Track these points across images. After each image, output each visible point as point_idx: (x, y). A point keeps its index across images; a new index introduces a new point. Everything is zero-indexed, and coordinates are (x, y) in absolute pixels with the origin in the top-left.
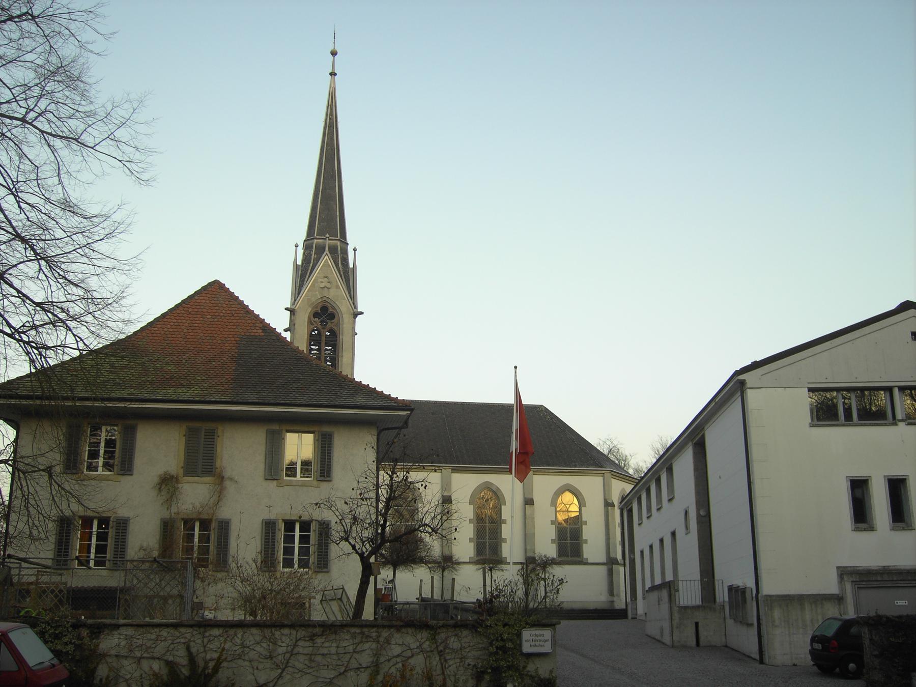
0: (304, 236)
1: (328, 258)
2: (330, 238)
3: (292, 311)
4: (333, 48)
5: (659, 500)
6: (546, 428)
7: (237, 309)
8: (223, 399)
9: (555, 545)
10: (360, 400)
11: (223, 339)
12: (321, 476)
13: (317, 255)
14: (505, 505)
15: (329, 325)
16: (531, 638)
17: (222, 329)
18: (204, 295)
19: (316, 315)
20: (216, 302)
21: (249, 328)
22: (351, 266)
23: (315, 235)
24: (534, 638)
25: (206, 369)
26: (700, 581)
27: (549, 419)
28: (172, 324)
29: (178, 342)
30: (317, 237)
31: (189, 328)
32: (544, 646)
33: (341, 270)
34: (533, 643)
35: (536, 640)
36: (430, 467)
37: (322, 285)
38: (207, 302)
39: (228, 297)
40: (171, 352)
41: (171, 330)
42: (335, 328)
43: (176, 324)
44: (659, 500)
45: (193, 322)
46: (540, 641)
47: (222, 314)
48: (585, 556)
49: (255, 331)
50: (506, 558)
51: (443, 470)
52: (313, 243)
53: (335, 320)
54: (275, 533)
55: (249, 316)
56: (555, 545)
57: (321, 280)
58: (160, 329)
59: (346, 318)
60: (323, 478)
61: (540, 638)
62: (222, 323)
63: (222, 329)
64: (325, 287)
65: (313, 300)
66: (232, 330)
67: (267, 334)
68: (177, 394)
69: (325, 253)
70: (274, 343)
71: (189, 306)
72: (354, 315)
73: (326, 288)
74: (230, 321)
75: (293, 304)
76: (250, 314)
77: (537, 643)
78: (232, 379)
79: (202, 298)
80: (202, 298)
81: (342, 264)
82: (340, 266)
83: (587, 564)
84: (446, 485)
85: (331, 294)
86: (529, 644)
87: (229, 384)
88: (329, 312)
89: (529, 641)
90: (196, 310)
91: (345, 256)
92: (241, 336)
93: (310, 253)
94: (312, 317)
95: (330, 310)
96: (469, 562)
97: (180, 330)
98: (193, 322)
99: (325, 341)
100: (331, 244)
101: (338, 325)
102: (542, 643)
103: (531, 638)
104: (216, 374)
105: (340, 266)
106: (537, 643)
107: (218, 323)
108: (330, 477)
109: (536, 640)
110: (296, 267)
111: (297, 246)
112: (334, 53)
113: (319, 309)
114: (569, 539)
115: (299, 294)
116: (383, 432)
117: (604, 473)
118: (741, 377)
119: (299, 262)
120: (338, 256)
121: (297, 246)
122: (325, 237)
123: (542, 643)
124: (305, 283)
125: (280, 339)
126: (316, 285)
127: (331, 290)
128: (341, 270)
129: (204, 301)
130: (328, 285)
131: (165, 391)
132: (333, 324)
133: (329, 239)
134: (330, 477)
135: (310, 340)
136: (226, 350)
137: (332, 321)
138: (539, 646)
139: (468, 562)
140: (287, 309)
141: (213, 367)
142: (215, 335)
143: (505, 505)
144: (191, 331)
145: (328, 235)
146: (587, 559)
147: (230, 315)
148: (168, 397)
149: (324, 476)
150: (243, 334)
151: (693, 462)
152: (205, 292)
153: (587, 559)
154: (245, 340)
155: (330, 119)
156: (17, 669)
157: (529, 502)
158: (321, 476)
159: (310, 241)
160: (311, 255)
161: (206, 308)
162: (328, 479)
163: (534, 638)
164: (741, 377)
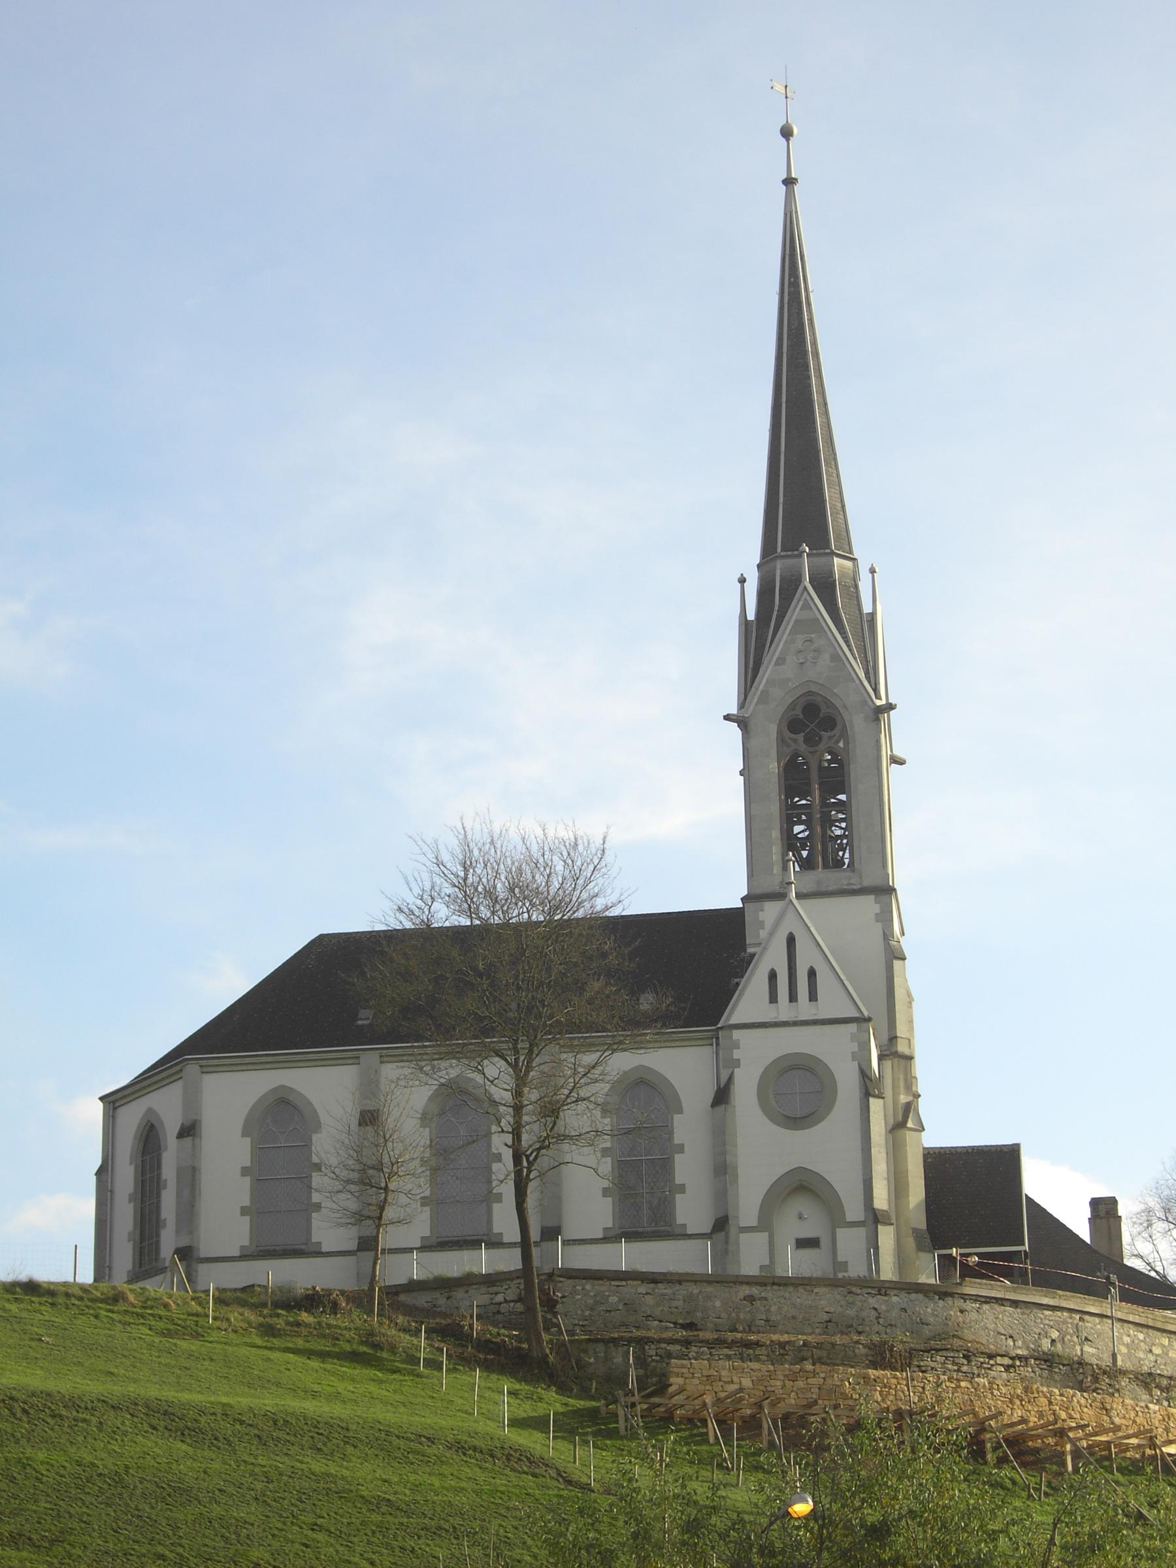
0: (756, 556)
1: (808, 598)
3: (741, 721)
4: (785, 122)
14: (681, 1112)
22: (867, 608)
23: (779, 550)
36: (410, 1051)
48: (680, 1220)
59: (857, 724)
69: (801, 588)
75: (742, 706)
83: (319, 1254)
84: (369, 1086)
88: (821, 715)
95: (824, 710)
96: (604, 1238)
110: (745, 624)
111: (742, 581)
112: (786, 133)
113: (798, 712)
115: (753, 682)
117: (358, 1058)
119: (751, 616)
121: (742, 581)
124: (765, 654)
135: (809, 772)
139: (601, 1239)
140: (727, 718)
143: (681, 1112)
146: (685, 1225)
153: (685, 1225)
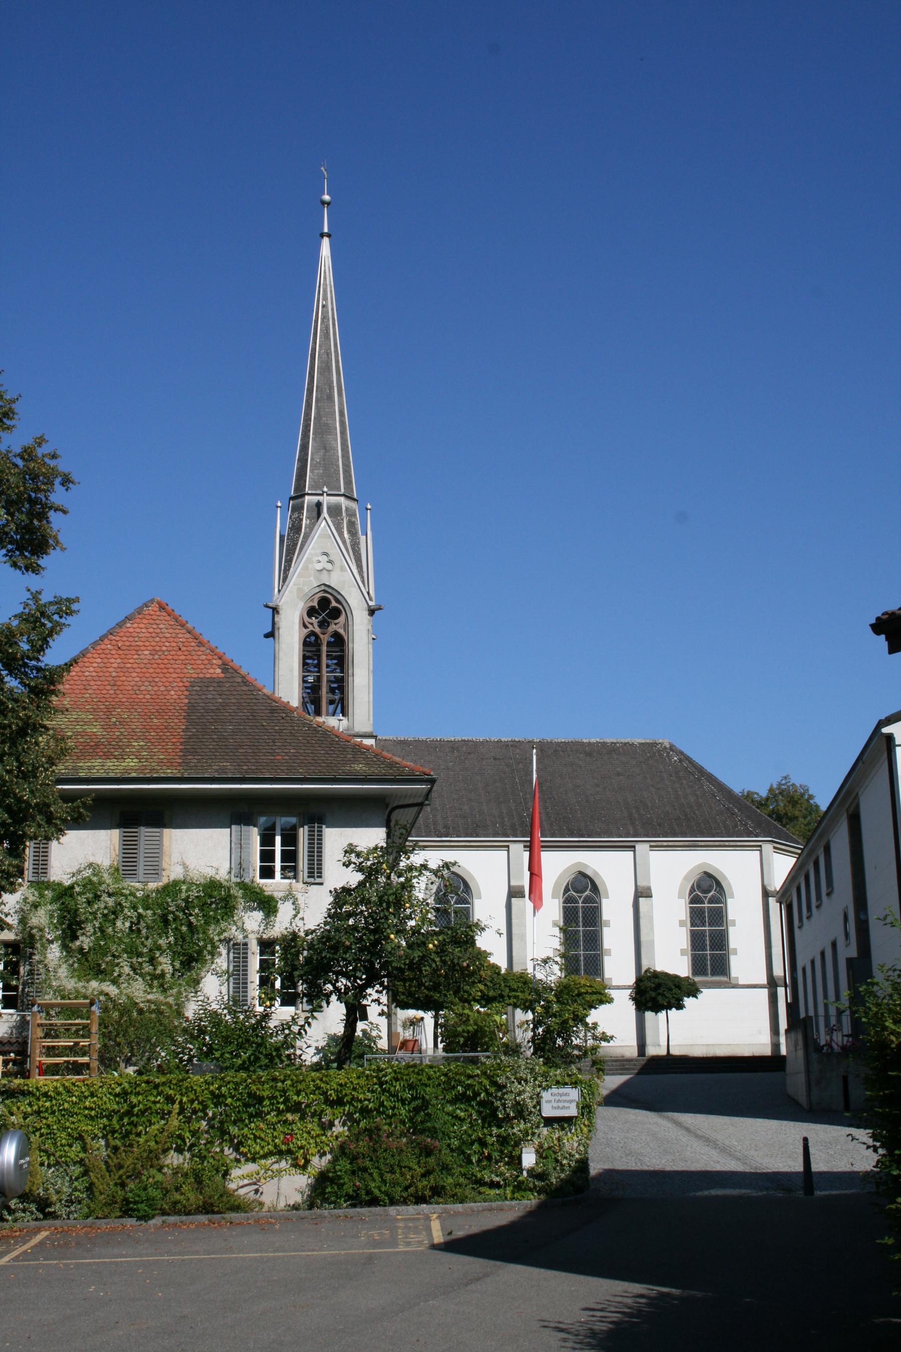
2: (329, 492)
5: (819, 897)
6: (671, 776)
7: (185, 640)
8: (169, 773)
9: (686, 957)
10: (360, 767)
11: (167, 684)
12: (309, 877)
13: (311, 520)
15: (332, 628)
16: (552, 1098)
17: (165, 671)
18: (138, 620)
19: (311, 612)
20: (156, 631)
21: (202, 666)
23: (307, 489)
24: (557, 1098)
25: (144, 730)
26: (849, 1017)
27: (676, 761)
28: (95, 665)
29: (104, 692)
30: (310, 492)
31: (119, 670)
32: (569, 1107)
33: (348, 541)
34: (556, 1105)
35: (559, 1101)
37: (319, 567)
38: (144, 630)
39: (173, 623)
40: (95, 707)
41: (94, 674)
42: (341, 631)
43: (102, 665)
44: (819, 897)
45: (125, 661)
46: (565, 1101)
47: (164, 648)
49: (212, 671)
50: (611, 979)
51: (512, 846)
52: (303, 502)
53: (342, 619)
54: (247, 958)
55: (202, 649)
56: (686, 957)
57: (317, 558)
58: (79, 674)
60: (312, 880)
61: (564, 1098)
62: (166, 661)
63: (165, 671)
64: (324, 569)
65: (306, 589)
66: (179, 671)
67: (229, 675)
68: (105, 768)
70: (239, 688)
71: (118, 638)
72: (369, 610)
73: (325, 572)
74: (176, 657)
76: (204, 646)
77: (561, 1105)
78: (182, 744)
79: (135, 625)
80: (135, 625)
81: (349, 532)
82: (346, 535)
85: (335, 580)
86: (550, 1105)
87: (178, 750)
89: (550, 1101)
90: (128, 643)
91: (353, 519)
92: (192, 680)
93: (298, 517)
94: (307, 619)
95: (334, 604)
97: (107, 674)
98: (125, 661)
99: (327, 652)
100: (332, 501)
101: (346, 626)
102: (566, 1105)
103: (552, 1098)
104: (158, 737)
105: (346, 535)
106: (561, 1105)
107: (160, 661)
108: (320, 877)
109: (559, 1101)
113: (315, 604)
114: (708, 948)
116: (397, 811)
118: (885, 730)
120: (343, 520)
122: (321, 492)
123: (566, 1105)
125: (247, 681)
126: (311, 566)
127: (332, 574)
128: (348, 541)
129: (139, 630)
130: (329, 566)
131: (90, 764)
132: (338, 626)
133: (328, 495)
134: (320, 877)
136: (173, 701)
137: (336, 621)
138: (563, 1108)
141: (155, 727)
142: (157, 680)
144: (122, 674)
145: (325, 489)
147: (177, 648)
148: (95, 774)
149: (313, 877)
150: (195, 676)
151: (850, 842)
152: (140, 616)
154: (198, 684)
155: (323, 306)
156: (641, 899)
157: (642, 893)
158: (309, 877)
159: (300, 500)
160: (302, 520)
161: (142, 639)
162: (318, 880)
163: (557, 1098)
164: (885, 730)
